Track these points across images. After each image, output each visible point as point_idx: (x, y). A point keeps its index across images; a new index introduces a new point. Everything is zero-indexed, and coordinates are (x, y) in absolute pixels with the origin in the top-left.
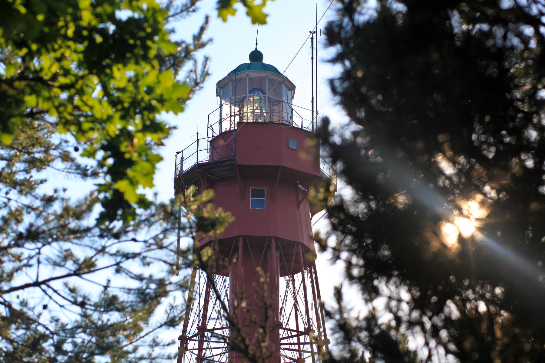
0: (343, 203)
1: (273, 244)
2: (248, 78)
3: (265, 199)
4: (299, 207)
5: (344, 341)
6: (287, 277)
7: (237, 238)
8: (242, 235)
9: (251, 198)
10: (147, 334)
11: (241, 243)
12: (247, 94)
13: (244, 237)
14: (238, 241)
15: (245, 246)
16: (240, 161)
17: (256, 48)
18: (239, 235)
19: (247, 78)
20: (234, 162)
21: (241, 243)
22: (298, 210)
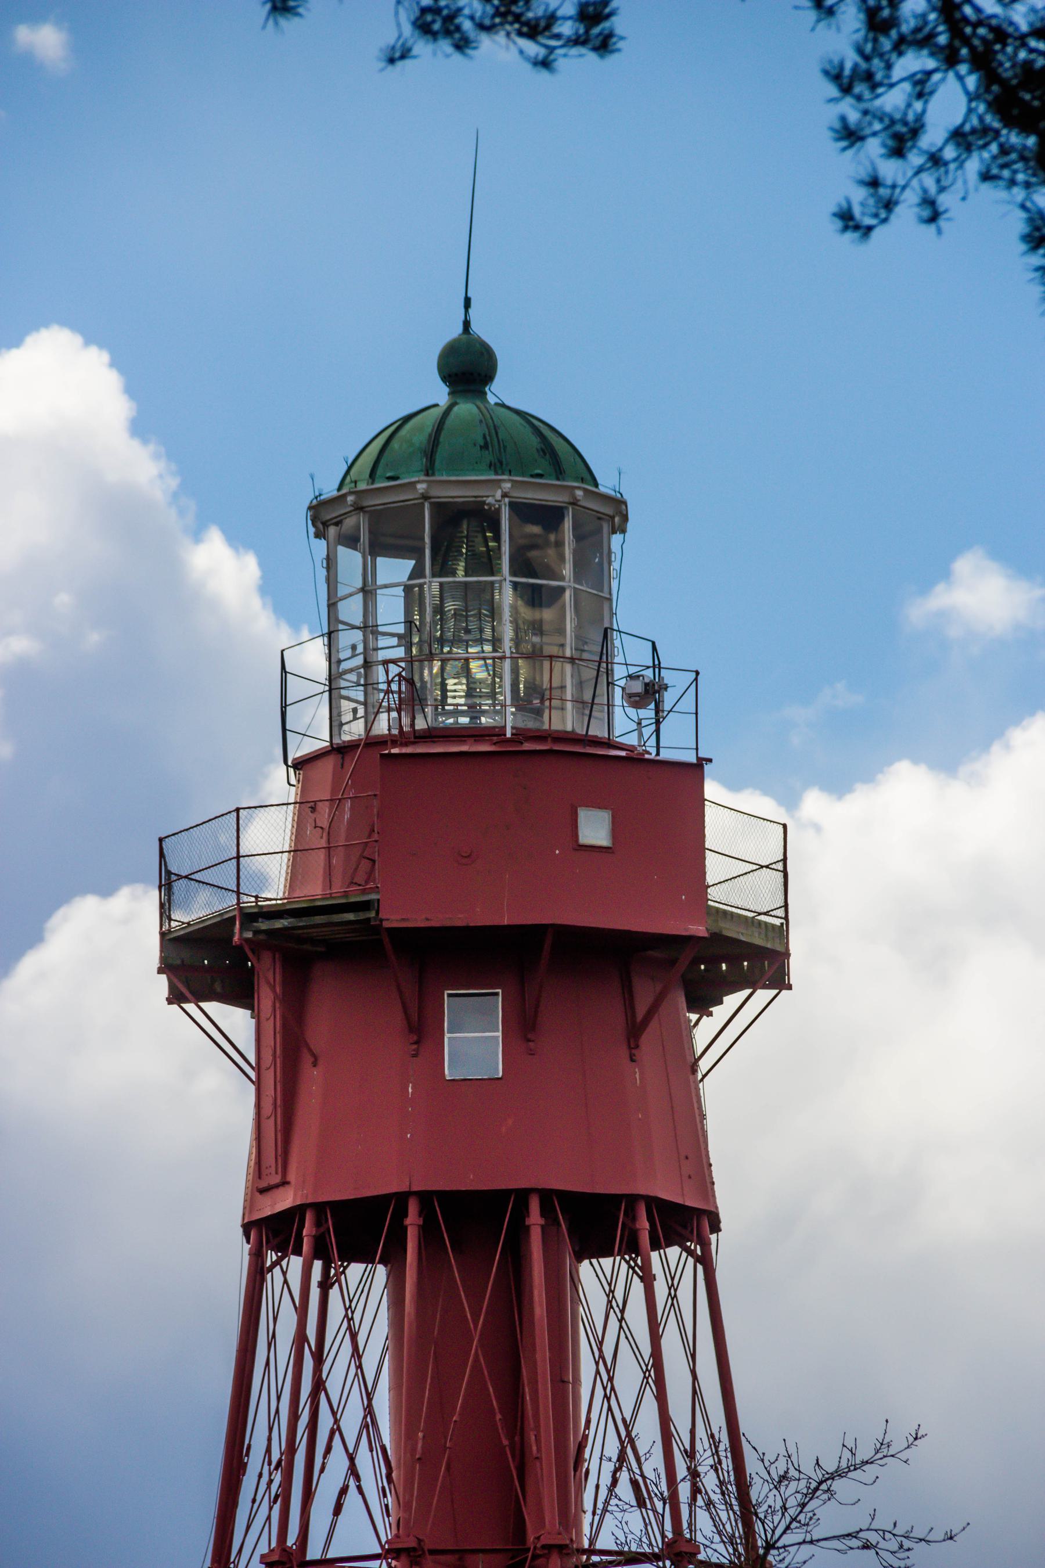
0: (920, 131)
1: (535, 1218)
2: (427, 505)
3: (500, 1034)
4: (637, 1046)
5: (982, 90)
6: (607, 1262)
7: (401, 1199)
8: (415, 1188)
9: (447, 1036)
10: (383, 595)
11: (412, 1219)
12: (425, 577)
13: (425, 1198)
14: (402, 1212)
15: (429, 1233)
16: (393, 917)
17: (467, 324)
18: (404, 1188)
19: (423, 504)
20: (373, 914)
21: (412, 1219)
22: (632, 1060)
